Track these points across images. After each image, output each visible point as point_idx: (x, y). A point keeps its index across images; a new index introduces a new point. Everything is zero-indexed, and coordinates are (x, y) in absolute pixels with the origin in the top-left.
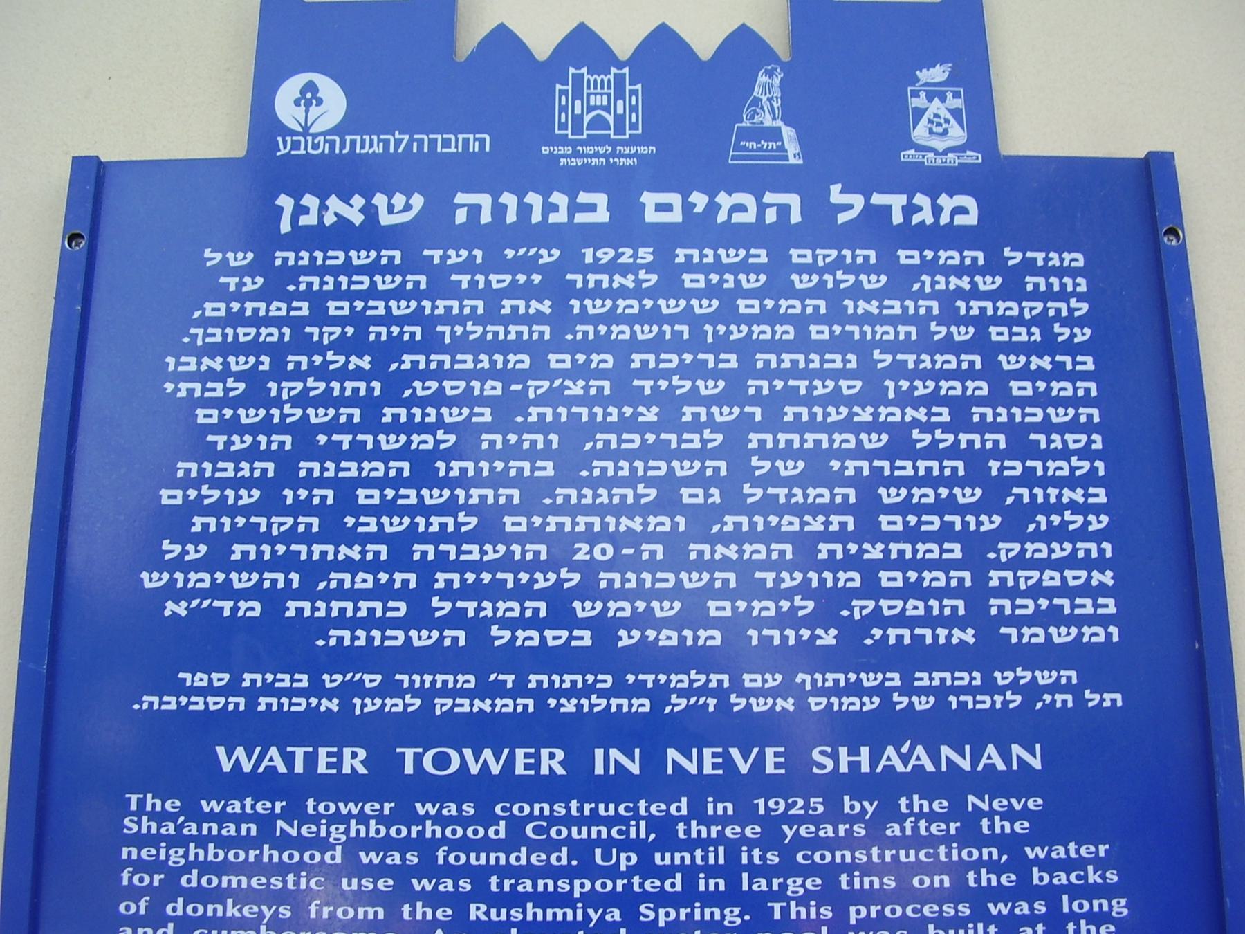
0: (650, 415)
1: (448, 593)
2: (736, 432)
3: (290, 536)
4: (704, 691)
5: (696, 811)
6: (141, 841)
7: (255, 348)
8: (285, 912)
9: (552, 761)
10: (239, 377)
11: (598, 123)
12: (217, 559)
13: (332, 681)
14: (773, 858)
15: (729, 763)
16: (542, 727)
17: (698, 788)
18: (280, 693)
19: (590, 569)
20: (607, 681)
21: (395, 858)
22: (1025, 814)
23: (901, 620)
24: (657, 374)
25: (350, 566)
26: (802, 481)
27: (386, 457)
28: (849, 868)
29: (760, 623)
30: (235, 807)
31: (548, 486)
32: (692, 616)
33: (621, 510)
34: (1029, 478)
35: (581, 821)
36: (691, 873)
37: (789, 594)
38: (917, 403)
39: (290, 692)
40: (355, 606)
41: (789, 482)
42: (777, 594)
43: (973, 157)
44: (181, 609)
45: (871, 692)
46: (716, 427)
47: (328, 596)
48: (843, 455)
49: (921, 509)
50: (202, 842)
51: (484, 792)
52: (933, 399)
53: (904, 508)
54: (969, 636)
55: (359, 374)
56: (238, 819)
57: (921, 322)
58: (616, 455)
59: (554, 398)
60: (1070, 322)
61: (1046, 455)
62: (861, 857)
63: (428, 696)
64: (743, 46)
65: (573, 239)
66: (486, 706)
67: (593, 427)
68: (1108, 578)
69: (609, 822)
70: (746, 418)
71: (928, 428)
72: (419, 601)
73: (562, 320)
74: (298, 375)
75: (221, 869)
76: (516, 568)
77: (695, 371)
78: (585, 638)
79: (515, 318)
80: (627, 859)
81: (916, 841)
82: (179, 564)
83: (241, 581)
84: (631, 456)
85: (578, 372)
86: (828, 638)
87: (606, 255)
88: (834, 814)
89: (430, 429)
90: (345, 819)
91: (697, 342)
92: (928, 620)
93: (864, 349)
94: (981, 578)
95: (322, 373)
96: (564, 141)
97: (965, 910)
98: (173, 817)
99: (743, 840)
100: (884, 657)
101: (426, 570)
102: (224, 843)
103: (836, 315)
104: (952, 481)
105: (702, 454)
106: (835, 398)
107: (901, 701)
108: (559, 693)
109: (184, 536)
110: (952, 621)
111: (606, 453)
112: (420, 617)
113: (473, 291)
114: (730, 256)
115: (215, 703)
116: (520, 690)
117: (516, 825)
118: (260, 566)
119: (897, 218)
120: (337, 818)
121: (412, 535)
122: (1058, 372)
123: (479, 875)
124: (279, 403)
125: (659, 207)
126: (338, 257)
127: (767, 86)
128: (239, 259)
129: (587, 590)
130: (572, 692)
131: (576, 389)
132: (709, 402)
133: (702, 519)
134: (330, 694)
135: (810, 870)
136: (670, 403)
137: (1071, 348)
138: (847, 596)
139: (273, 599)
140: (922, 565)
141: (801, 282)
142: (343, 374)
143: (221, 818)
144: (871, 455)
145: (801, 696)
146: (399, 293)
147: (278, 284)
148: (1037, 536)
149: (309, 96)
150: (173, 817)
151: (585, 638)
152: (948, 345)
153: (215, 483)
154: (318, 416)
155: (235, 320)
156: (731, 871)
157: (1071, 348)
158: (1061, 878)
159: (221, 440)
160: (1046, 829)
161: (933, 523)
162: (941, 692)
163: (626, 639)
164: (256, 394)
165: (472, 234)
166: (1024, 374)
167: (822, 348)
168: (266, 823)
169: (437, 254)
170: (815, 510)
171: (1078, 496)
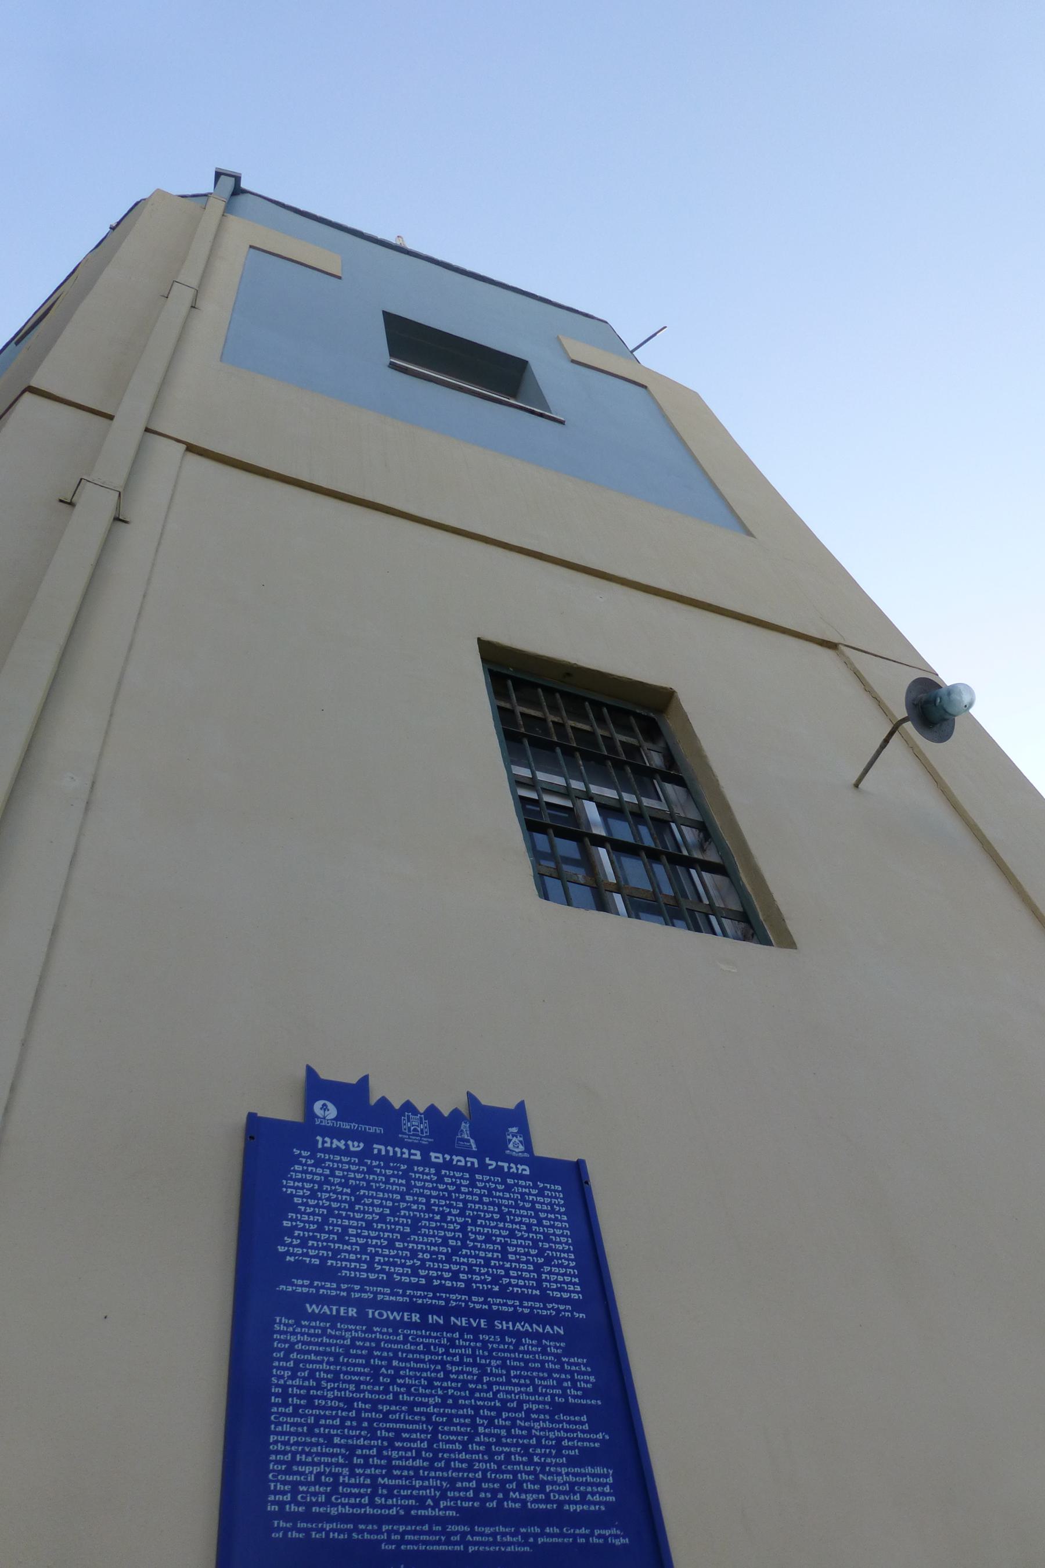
0: (438, 1217)
1: (379, 1263)
2: (464, 1225)
3: (327, 1240)
4: (460, 1300)
5: (461, 1337)
6: (281, 1333)
7: (311, 1181)
8: (332, 1359)
9: (416, 1318)
10: (308, 1189)
11: (415, 1130)
12: (303, 1244)
13: (344, 1286)
14: (486, 1353)
15: (470, 1323)
16: (411, 1307)
17: (462, 1330)
18: (327, 1289)
19: (423, 1261)
20: (431, 1295)
21: (367, 1344)
22: (560, 1347)
23: (517, 1286)
24: (439, 1206)
25: (349, 1252)
26: (485, 1242)
27: (358, 1220)
28: (510, 1359)
29: (476, 1282)
30: (313, 1324)
31: (409, 1235)
32: (455, 1277)
33: (431, 1244)
34: (550, 1249)
35: (426, 1337)
36: (461, 1356)
37: (484, 1274)
38: (516, 1223)
39: (331, 1289)
40: (350, 1264)
41: (481, 1242)
42: (480, 1274)
43: (526, 1155)
44: (292, 1259)
45: (511, 1306)
46: (458, 1223)
47: (341, 1260)
48: (496, 1236)
49: (520, 1254)
50: (302, 1334)
51: (396, 1325)
52: (520, 1223)
53: (515, 1253)
54: (538, 1292)
55: (346, 1194)
56: (315, 1328)
57: (516, 1200)
58: (429, 1228)
59: (408, 1209)
60: (558, 1205)
61: (555, 1243)
62: (513, 1355)
63: (376, 1294)
64: (456, 1112)
65: (410, 1163)
66: (394, 1298)
67: (420, 1219)
68: (577, 1280)
69: (436, 1338)
70: (466, 1222)
71: (520, 1231)
72: (371, 1264)
73: (409, 1187)
74: (326, 1191)
75: (309, 1343)
76: (401, 1258)
77: (450, 1206)
78: (423, 1281)
79: (393, 1184)
80: (441, 1350)
81: (528, 1352)
82: (290, 1245)
83: (312, 1252)
84: (433, 1229)
85: (415, 1202)
86: (496, 1289)
87: (421, 1169)
88: (503, 1341)
89: (371, 1213)
90: (351, 1330)
91: (450, 1198)
92: (525, 1286)
93: (499, 1206)
94: (539, 1276)
95: (335, 1192)
96: (405, 1134)
97: (546, 1375)
98: (291, 1325)
99: (476, 1347)
100: (513, 1296)
101: (373, 1256)
102: (310, 1335)
103: (490, 1195)
104: (528, 1247)
105: (454, 1230)
106: (492, 1219)
107: (520, 1310)
108: (417, 1297)
109: (292, 1237)
110: (532, 1288)
111: (425, 1227)
112: (371, 1269)
113: (380, 1174)
114: (458, 1174)
115: (305, 1290)
116: (404, 1295)
117: (406, 1336)
118: (317, 1248)
119: (506, 1170)
120: (347, 1330)
121: (366, 1245)
122: (556, 1219)
123: (396, 1351)
124: (321, 1199)
125: (436, 1157)
126: (338, 1158)
127: (465, 1126)
128: (305, 1153)
129: (423, 1266)
130: (420, 1297)
131: (415, 1207)
132: (455, 1215)
133: (456, 1251)
134: (344, 1290)
135: (497, 1358)
136: (444, 1216)
137: (559, 1212)
138: (501, 1277)
139: (324, 1260)
140: (522, 1270)
141: (479, 1184)
142: (342, 1193)
143: (309, 1327)
144: (504, 1237)
145: (490, 1305)
146: (358, 1171)
147: (319, 1163)
148: (554, 1266)
149: (324, 1107)
150: (291, 1325)
151: (423, 1281)
152: (523, 1208)
153: (301, 1221)
154: (334, 1205)
155: (306, 1172)
156: (474, 1356)
157: (559, 1212)
158: (574, 1368)
159: (303, 1208)
160: (568, 1352)
161: (524, 1258)
162: (532, 1308)
163: (436, 1283)
164: (313, 1195)
165: (378, 1157)
166: (546, 1218)
167: (487, 1204)
168: (324, 1329)
169: (369, 1162)
170: (489, 1251)
171: (566, 1255)
